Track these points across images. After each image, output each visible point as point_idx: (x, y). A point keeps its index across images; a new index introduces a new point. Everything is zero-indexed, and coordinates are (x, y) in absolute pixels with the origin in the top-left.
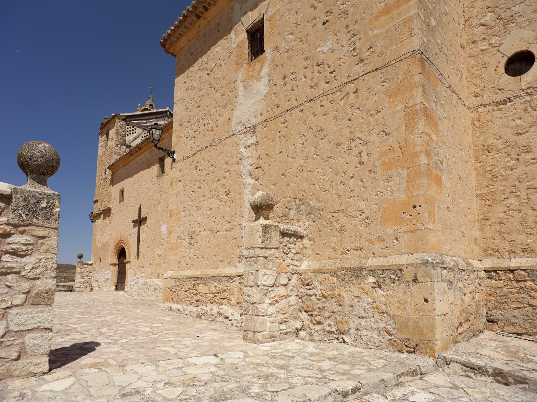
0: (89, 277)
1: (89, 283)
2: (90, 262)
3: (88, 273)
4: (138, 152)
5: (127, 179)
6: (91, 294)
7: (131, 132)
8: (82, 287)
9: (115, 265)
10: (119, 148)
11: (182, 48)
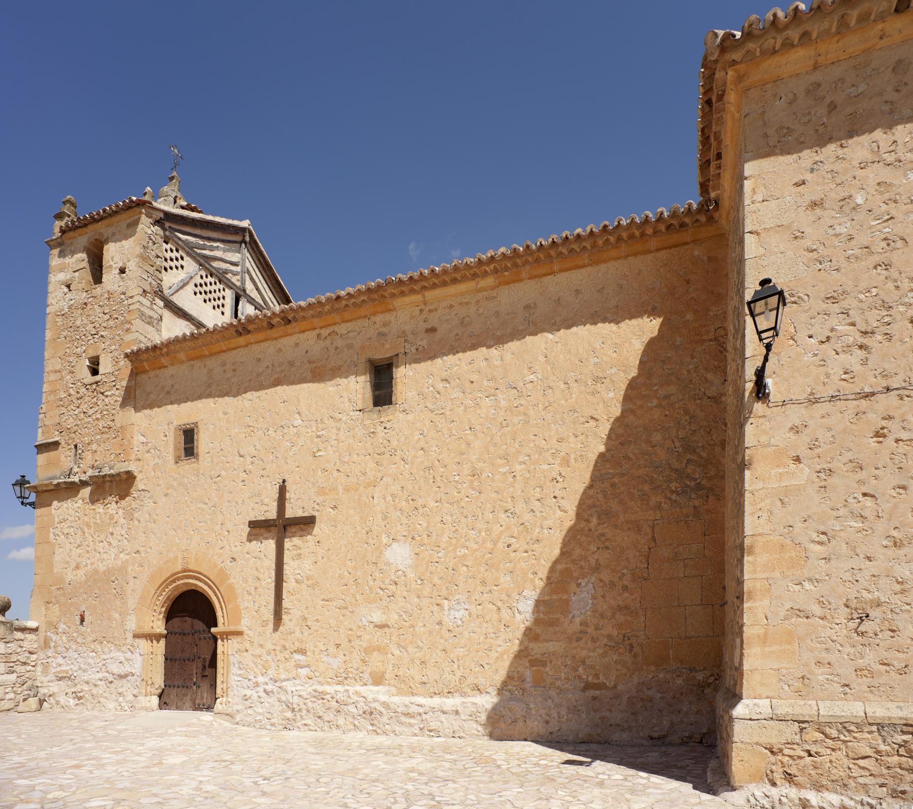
1: (29, 683)
2: (32, 624)
3: (27, 654)
4: (274, 330)
5: (211, 401)
6: (38, 715)
7: (173, 264)
8: (8, 696)
9: (152, 637)
10: (148, 303)
11: (777, 80)
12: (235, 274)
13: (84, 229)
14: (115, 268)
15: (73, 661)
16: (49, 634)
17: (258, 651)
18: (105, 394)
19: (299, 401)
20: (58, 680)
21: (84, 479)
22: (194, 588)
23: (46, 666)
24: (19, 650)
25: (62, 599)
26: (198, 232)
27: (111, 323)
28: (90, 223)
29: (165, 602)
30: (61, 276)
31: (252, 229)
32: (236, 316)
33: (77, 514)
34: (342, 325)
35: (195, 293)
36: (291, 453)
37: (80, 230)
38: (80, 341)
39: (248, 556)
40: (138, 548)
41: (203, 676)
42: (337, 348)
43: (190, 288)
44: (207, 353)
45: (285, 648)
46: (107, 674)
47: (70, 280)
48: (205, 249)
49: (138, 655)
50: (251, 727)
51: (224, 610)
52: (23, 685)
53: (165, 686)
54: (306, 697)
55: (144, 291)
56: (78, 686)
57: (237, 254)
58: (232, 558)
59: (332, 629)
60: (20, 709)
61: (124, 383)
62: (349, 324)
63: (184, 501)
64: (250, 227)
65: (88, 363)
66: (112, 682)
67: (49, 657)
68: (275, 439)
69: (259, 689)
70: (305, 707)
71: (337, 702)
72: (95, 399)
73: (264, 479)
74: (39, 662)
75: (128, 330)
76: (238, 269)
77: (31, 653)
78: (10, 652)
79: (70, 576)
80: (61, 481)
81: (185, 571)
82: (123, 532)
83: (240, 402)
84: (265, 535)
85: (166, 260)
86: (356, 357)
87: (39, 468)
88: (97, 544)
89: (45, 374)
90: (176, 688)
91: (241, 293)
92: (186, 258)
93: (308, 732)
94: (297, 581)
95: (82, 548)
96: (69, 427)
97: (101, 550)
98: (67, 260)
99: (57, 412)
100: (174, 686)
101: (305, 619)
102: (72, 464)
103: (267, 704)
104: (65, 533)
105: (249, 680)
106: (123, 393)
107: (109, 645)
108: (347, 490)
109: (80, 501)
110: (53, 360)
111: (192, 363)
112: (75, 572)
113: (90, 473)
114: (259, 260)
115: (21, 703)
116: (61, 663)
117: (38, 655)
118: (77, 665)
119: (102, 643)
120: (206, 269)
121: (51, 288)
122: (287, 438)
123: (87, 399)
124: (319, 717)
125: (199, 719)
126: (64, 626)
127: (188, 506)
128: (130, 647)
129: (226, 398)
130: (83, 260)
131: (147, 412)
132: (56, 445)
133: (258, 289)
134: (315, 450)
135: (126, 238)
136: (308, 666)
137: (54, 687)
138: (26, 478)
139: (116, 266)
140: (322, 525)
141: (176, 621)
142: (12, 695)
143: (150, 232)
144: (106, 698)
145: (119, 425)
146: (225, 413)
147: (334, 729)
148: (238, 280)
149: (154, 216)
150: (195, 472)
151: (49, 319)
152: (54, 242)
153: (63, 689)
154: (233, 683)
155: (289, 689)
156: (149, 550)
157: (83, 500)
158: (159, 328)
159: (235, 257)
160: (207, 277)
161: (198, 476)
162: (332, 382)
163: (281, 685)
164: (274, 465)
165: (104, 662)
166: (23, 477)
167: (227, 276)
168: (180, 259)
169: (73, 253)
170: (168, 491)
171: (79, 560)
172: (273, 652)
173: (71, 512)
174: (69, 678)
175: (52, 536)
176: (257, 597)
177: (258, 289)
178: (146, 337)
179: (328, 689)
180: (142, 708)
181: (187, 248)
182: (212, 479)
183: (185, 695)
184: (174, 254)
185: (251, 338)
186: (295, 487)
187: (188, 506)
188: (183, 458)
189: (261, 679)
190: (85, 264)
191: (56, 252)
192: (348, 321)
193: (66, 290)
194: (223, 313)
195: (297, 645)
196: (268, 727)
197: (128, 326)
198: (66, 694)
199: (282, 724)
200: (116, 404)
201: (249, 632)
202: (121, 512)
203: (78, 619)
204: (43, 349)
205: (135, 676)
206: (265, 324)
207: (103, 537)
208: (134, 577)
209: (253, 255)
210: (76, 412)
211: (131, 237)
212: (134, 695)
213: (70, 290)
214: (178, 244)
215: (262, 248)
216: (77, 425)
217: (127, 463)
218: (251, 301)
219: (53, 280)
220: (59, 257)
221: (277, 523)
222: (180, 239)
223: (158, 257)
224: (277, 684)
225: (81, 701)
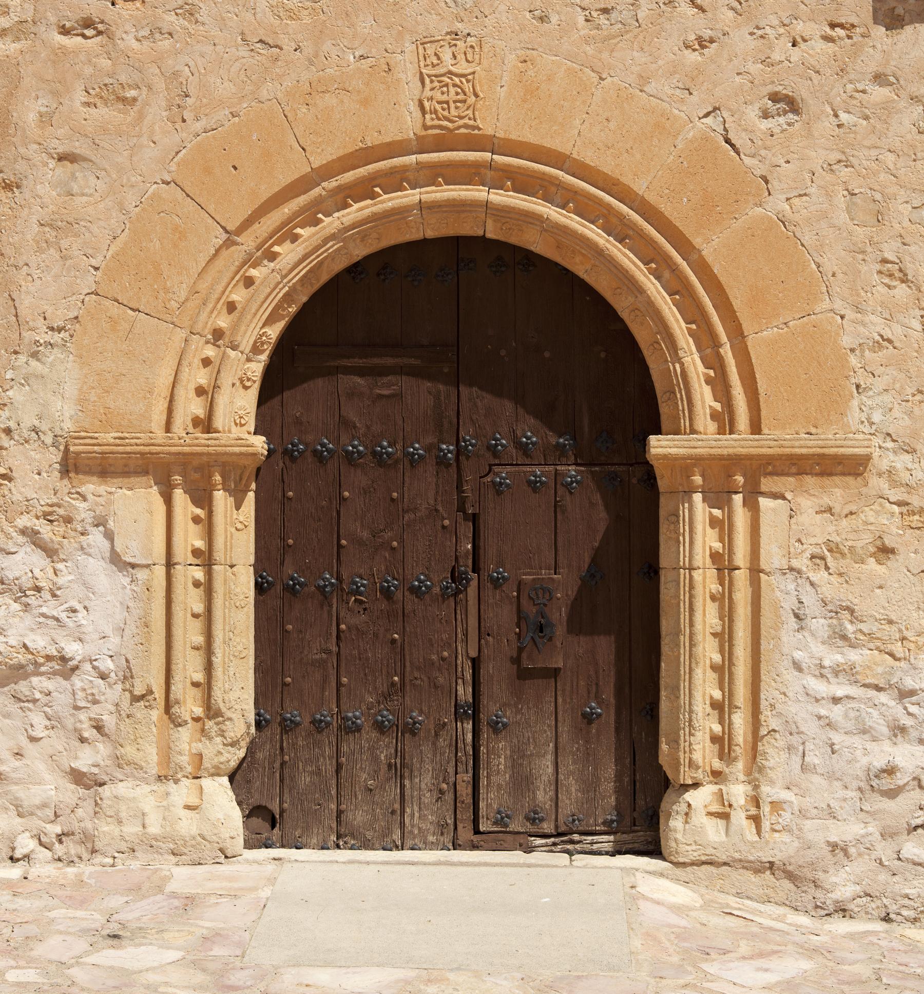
41: (524, 674)
58: (775, 98)
90: (328, 739)
100: (318, 726)
201: (902, 461)
212: (78, 777)
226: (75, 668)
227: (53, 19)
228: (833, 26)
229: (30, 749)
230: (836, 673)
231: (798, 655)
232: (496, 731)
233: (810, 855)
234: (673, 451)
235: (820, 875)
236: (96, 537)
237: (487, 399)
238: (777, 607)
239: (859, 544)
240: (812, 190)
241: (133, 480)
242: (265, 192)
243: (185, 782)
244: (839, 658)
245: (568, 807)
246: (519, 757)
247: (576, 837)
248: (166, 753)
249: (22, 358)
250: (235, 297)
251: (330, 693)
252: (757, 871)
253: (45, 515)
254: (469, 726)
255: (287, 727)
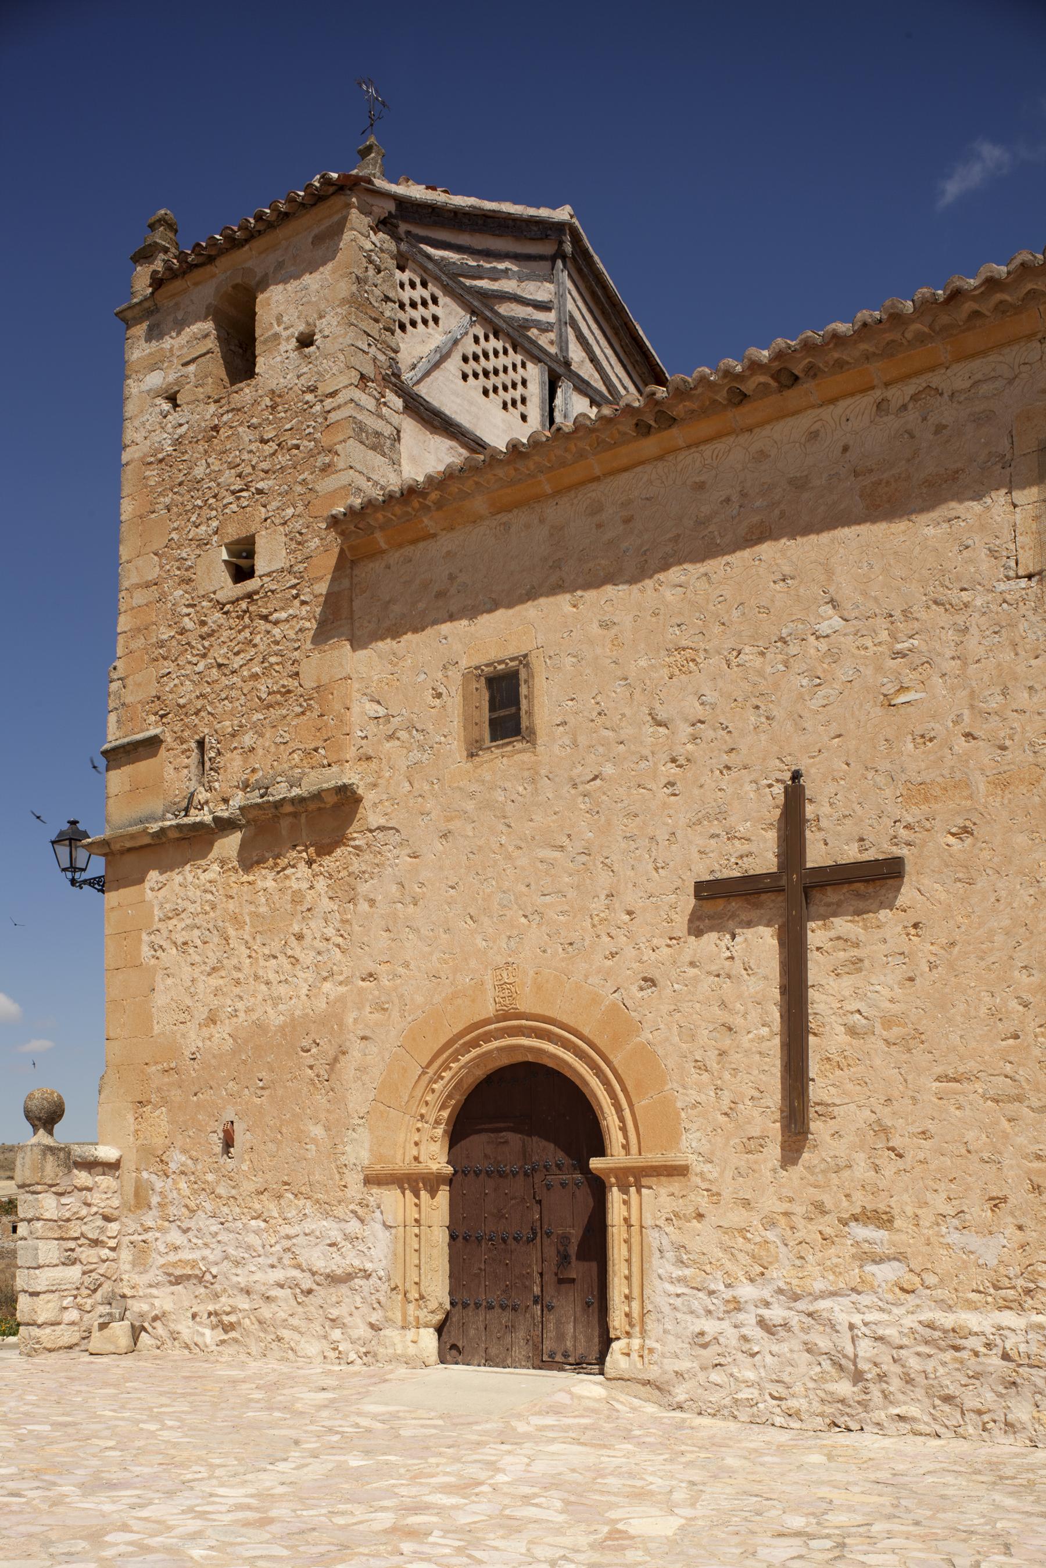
0: (105, 1253)
1: (107, 1287)
2: (107, 1152)
3: (100, 1222)
4: (746, 408)
5: (563, 602)
7: (416, 314)
10: (369, 403)
12: (546, 328)
13: (209, 268)
14: (288, 339)
15: (208, 1239)
16: (145, 1175)
17: (736, 1217)
18: (272, 618)
19: (829, 573)
20: (171, 1283)
21: (226, 815)
22: (530, 1058)
23: (142, 1252)
24: (84, 1211)
25: (176, 1096)
26: (464, 239)
27: (283, 459)
28: (223, 251)
29: (450, 1097)
30: (155, 380)
31: (577, 224)
32: (552, 421)
33: (209, 896)
34: (955, 367)
35: (465, 377)
36: (815, 704)
37: (197, 274)
38: (205, 511)
39: (695, 971)
40: (371, 967)
41: (561, 1281)
42: (940, 428)
43: (453, 365)
44: (548, 489)
45: (820, 1209)
46: (296, 1273)
47: (177, 382)
48: (481, 278)
49: (378, 1227)
50: (725, 1418)
51: (627, 1113)
52: (95, 1291)
53: (452, 1304)
54: (898, 1341)
55: (363, 377)
56: (223, 1299)
57: (547, 285)
58: (645, 979)
59: (974, 1157)
60: (94, 1345)
61: (322, 588)
62: (976, 364)
63: (495, 847)
64: (574, 220)
65: (225, 556)
66: (310, 1292)
67: (147, 1230)
68: (761, 673)
69: (741, 1317)
70: (896, 1369)
71: (1006, 1357)
72: (246, 634)
73: (734, 774)
74: (126, 1240)
75: (326, 469)
76: (551, 317)
77: (107, 1219)
78: (68, 1215)
79: (193, 1039)
80: (168, 823)
81: (506, 1017)
82: (330, 932)
83: (650, 592)
84: (745, 916)
85: (402, 306)
86: (1006, 442)
87: (111, 801)
88: (262, 963)
89: (123, 594)
90: (482, 1311)
91: (560, 370)
92: (443, 300)
93: (911, 1438)
94: (852, 1031)
95: (223, 973)
96: (182, 701)
97: (272, 976)
98: (167, 343)
99: (152, 672)
100: (477, 1306)
101: (882, 1130)
102: (193, 785)
103: (769, 1359)
104: (179, 942)
105: (711, 1293)
106: (318, 610)
107: (301, 1202)
108: (1002, 783)
109: (216, 867)
110: (140, 562)
111: (504, 517)
112: (205, 1032)
113: (238, 800)
114: (593, 294)
115: (96, 1334)
116: (178, 1243)
117: (123, 1224)
118: (219, 1249)
119: (280, 1197)
120: (485, 321)
121: (130, 408)
122: (797, 666)
123: (225, 634)
124: (948, 1399)
125: (570, 1393)
126: (183, 1158)
127: (509, 857)
128: (358, 1208)
129: (609, 589)
130: (206, 336)
131: (385, 646)
132: (153, 744)
133: (593, 359)
134: (889, 688)
135: (312, 267)
136: (899, 1257)
137: (165, 1300)
138: (81, 827)
139: (289, 332)
140: (926, 882)
141: (478, 1143)
142: (73, 1315)
143: (369, 246)
144: (295, 1329)
145: (309, 684)
146: (604, 625)
147: (996, 1432)
148: (552, 343)
149: (375, 209)
150: (526, 774)
151: (129, 477)
152: (136, 311)
153: (186, 1304)
154: (662, 1301)
155: (842, 1318)
156: (401, 970)
157: (223, 863)
158: (395, 457)
159: (542, 292)
160: (487, 338)
161: (533, 781)
162: (934, 515)
163: (811, 1309)
164: (763, 737)
165: (287, 1243)
166: (74, 823)
167: (529, 334)
168: (430, 302)
169: (180, 325)
170: (451, 826)
171: (216, 1002)
172: (783, 1221)
173: (193, 893)
174: (200, 1279)
175: (146, 951)
176: (727, 1076)
177: (593, 359)
178: (369, 479)
179: (972, 1320)
180: (395, 1359)
181: (444, 278)
182: (575, 786)
183: (511, 1328)
184: (419, 293)
185: (676, 435)
186: (831, 788)
187: (509, 857)
188: (488, 743)
189: (746, 1291)
190: (211, 343)
191: (140, 330)
192: (973, 356)
193: (166, 406)
194: (524, 418)
195: (861, 1200)
196: (779, 1420)
197: (327, 460)
198: (194, 1316)
199: (822, 1415)
200: (300, 636)
201: (707, 1168)
202: (321, 884)
203: (216, 1142)
204: (115, 540)
205: (374, 1279)
206: (722, 396)
207: (275, 946)
208: (363, 1038)
209: (580, 283)
210: (200, 667)
211: (324, 263)
212: (372, 1326)
213: (176, 406)
214: (425, 269)
215: (601, 266)
216: (202, 696)
217: (335, 769)
218: (583, 387)
219: (134, 391)
220: (149, 339)
221: (783, 882)
222: (429, 257)
223: (387, 299)
224: (801, 1305)
225: (233, 1334)
226: (370, 1275)
227: (358, 975)
228: (671, 939)
229: (355, 1312)
230: (679, 1281)
231: (660, 1271)
232: (549, 1310)
233: (666, 1377)
234: (599, 1166)
235: (671, 1388)
236: (378, 1213)
237: (544, 1143)
238: (650, 1246)
239: (688, 1212)
240: (661, 1026)
241: (390, 1187)
242: (436, 1048)
243: (413, 1330)
244: (680, 1273)
245: (581, 1350)
246: (559, 1323)
247: (584, 1366)
248: (405, 1315)
249: (350, 1131)
250: (428, 1098)
251: (482, 1289)
252: (644, 1385)
253: (360, 1203)
254: (539, 1307)
255: (465, 1306)
